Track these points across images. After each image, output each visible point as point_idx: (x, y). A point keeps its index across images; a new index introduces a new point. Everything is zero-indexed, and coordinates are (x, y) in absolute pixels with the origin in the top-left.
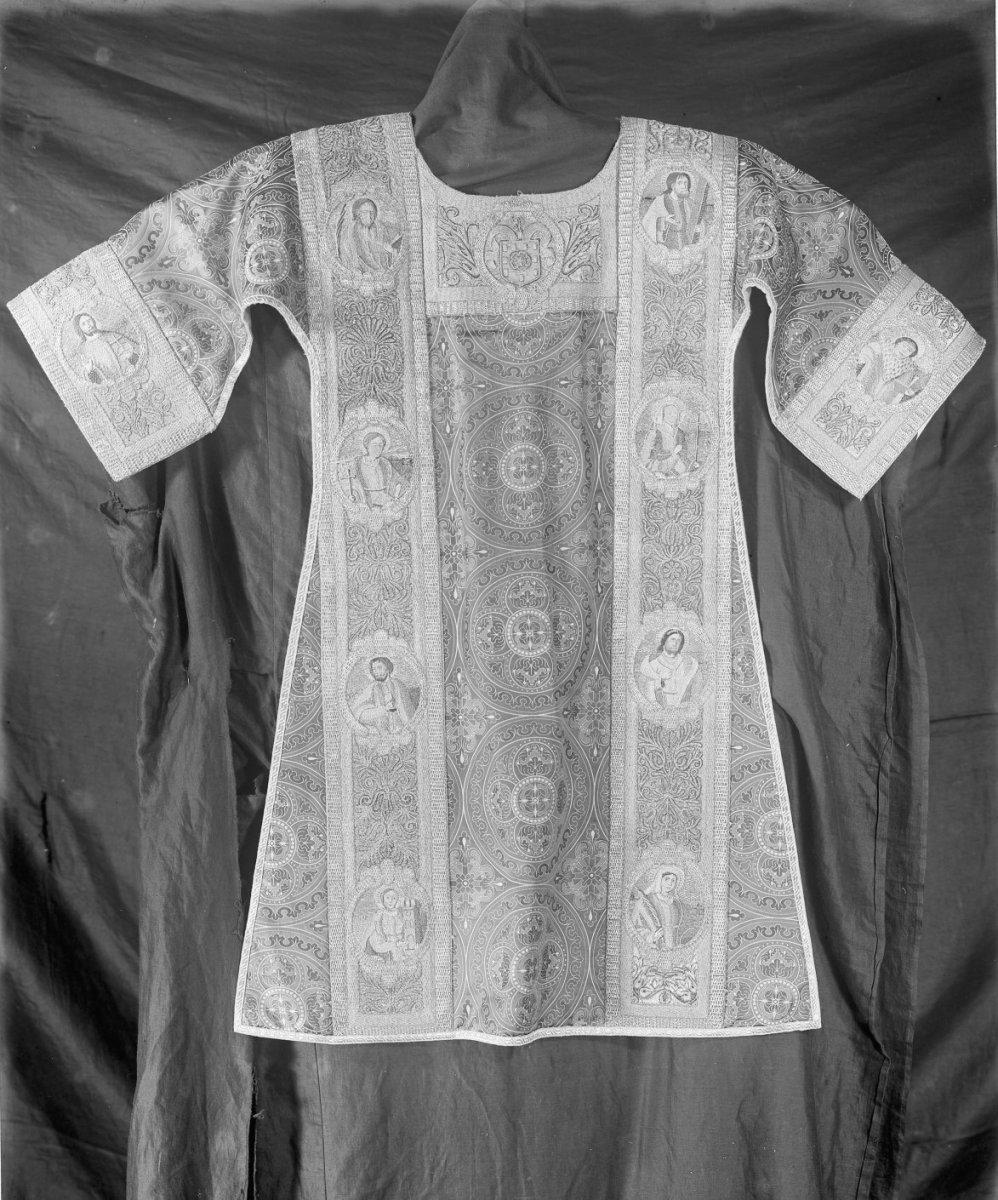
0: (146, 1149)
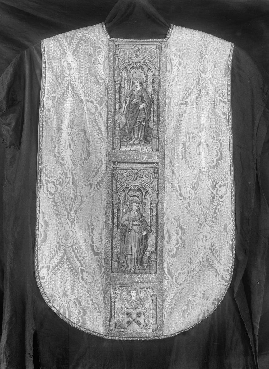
0: (4, 357)
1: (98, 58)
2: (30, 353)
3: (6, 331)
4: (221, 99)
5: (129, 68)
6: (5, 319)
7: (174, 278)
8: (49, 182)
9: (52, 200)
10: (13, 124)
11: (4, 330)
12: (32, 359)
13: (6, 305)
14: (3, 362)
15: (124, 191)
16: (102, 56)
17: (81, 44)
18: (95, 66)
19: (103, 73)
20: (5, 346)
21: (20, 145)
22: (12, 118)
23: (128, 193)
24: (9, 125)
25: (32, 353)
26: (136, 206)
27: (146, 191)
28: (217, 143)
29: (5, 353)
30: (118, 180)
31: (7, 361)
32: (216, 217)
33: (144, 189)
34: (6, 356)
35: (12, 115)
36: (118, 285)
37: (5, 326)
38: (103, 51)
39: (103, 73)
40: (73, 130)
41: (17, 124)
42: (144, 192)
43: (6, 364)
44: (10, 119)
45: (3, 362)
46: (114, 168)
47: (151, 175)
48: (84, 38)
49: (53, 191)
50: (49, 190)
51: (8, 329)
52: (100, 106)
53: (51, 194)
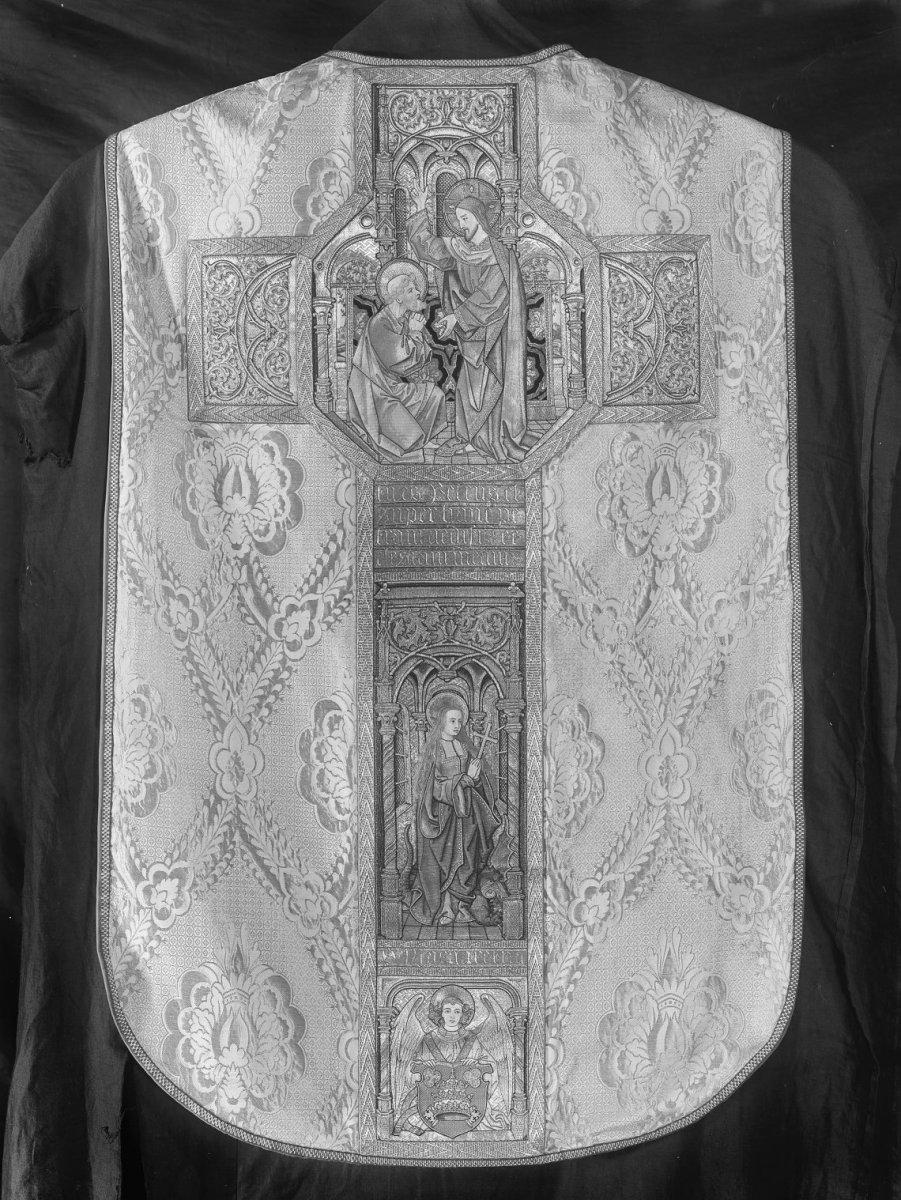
0: (20, 1136)
1: (331, 740)
2: (107, 1128)
3: (29, 1054)
4: (731, 870)
5: (420, 158)
6: (24, 1014)
7: (274, 618)
8: (174, 597)
9: (185, 653)
10: (49, 387)
11: (22, 1052)
12: (116, 1146)
13: (30, 969)
14: (19, 1151)
15: (412, 674)
16: (342, 736)
17: (276, 693)
18: (321, 766)
19: (347, 791)
20: (24, 1102)
21: (71, 449)
22: (42, 363)
23: (425, 683)
24: (37, 387)
25: (114, 1127)
26: (456, 721)
27: (484, 674)
28: (710, 469)
29: (25, 1123)
30: (393, 640)
31: (30, 1151)
32: (700, 166)
33: (478, 669)
34: (26, 1133)
35: (45, 351)
36: (401, 978)
37: (24, 1036)
38: (343, 175)
39: (347, 791)
40: (248, 982)
41: (60, 385)
42: (478, 681)
43: (29, 1160)
44: (40, 370)
45: (19, 1151)
46: (379, 602)
47: (497, 621)
48: (285, 675)
49: (185, 624)
50: (174, 621)
51: (36, 1046)
52: (340, 900)
53: (180, 635)
